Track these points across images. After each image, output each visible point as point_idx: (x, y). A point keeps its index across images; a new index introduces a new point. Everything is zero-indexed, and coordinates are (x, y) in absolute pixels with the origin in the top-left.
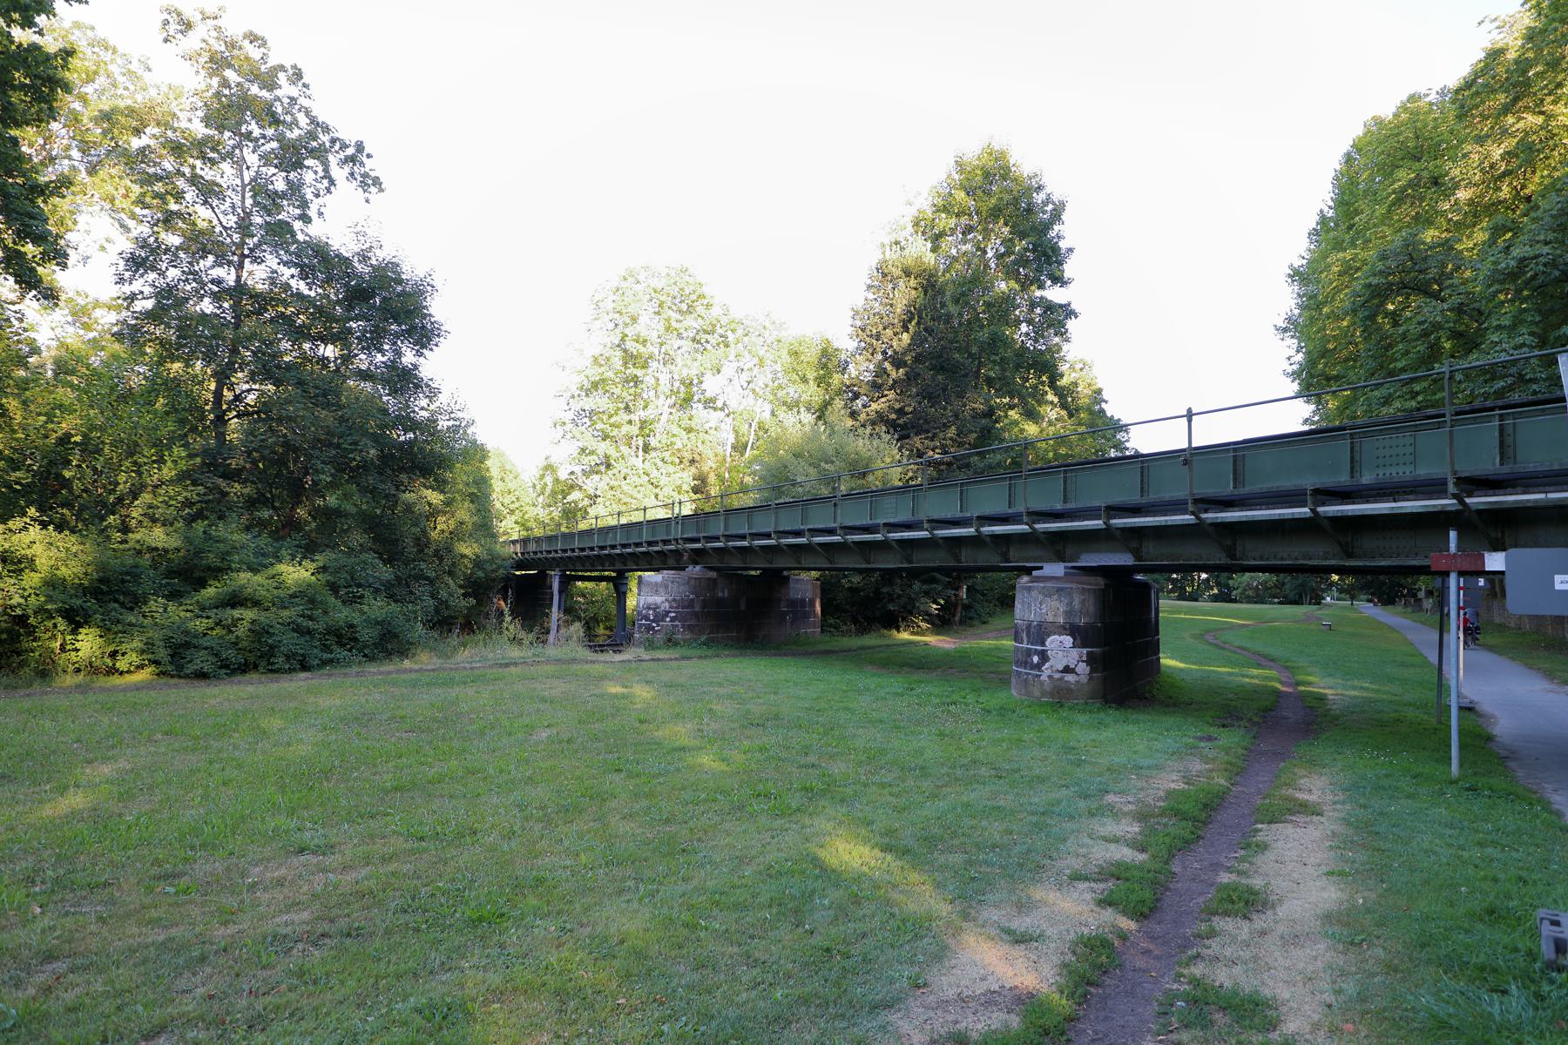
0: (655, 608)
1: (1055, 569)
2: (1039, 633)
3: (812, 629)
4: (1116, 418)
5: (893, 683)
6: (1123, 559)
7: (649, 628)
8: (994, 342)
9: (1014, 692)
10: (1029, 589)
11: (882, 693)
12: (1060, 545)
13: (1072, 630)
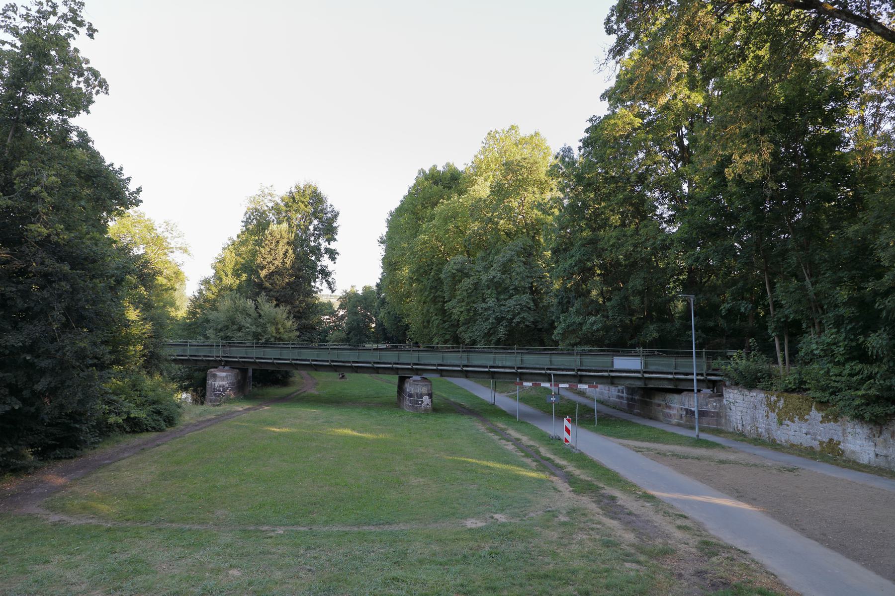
0: (223, 386)
1: (418, 378)
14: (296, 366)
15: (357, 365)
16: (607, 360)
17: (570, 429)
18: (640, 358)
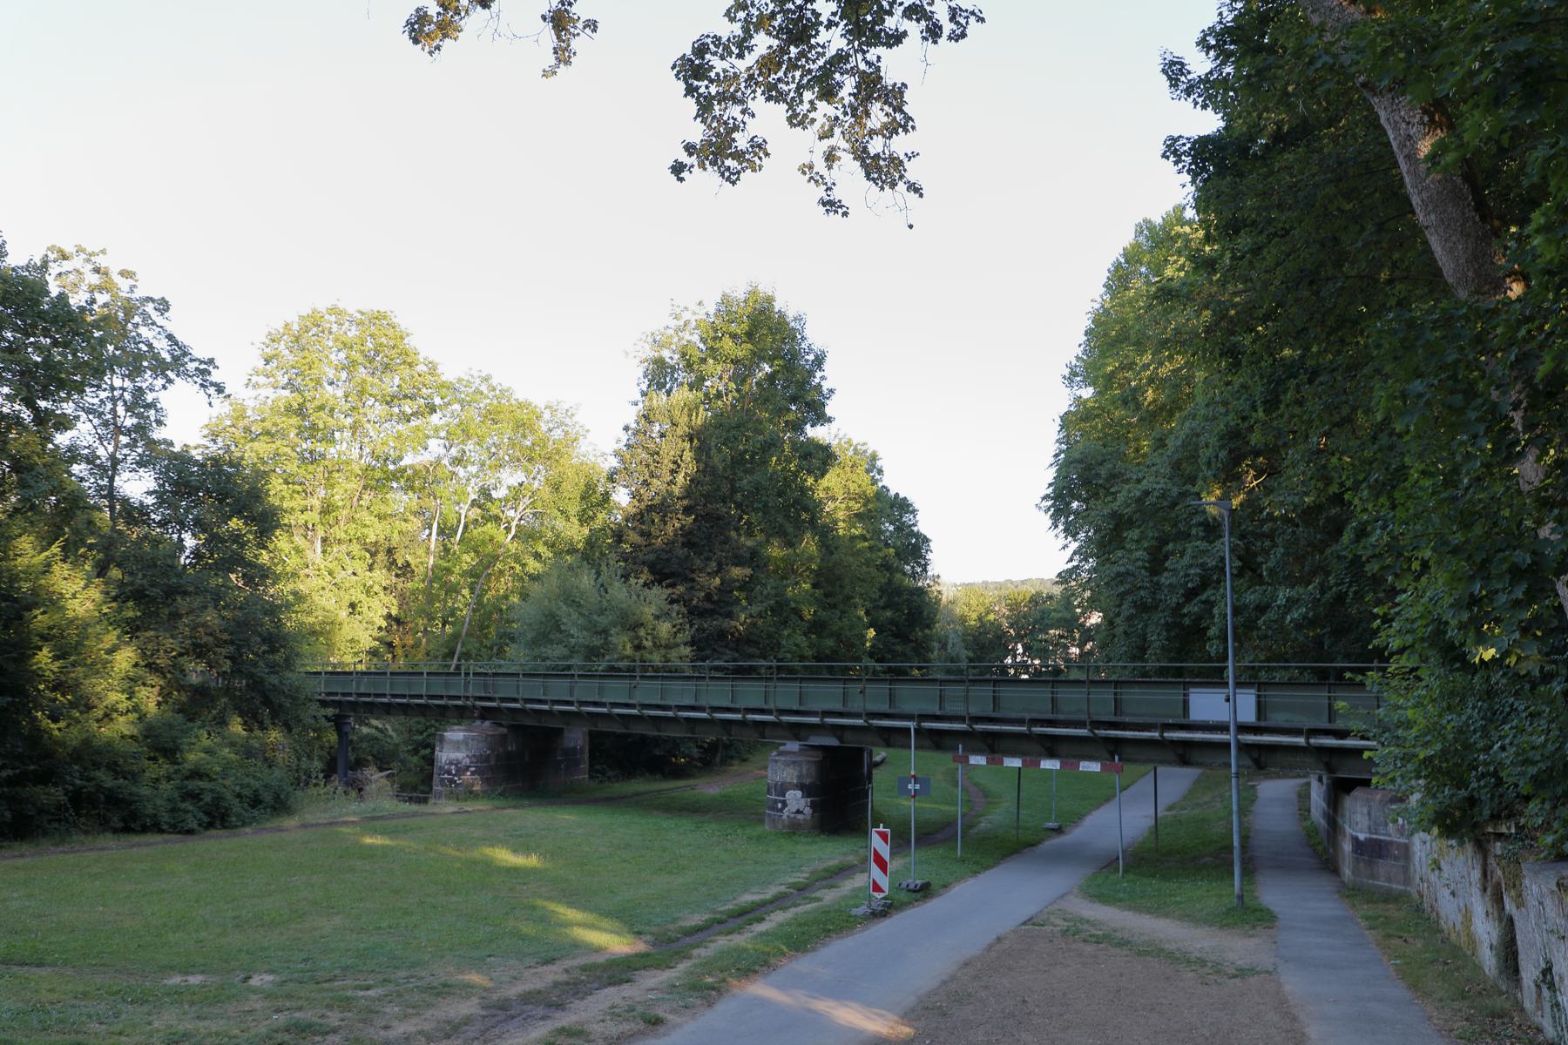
0: (457, 763)
1: (793, 746)
2: (782, 789)
3: (582, 775)
4: (901, 496)
5: (686, 823)
6: (832, 742)
7: (452, 781)
8: (757, 489)
9: (767, 827)
10: (776, 761)
11: (681, 830)
12: (797, 731)
13: (801, 787)
14: (891, 737)
15: (996, 728)
16: (1175, 695)
17: (887, 858)
18: (1253, 691)
